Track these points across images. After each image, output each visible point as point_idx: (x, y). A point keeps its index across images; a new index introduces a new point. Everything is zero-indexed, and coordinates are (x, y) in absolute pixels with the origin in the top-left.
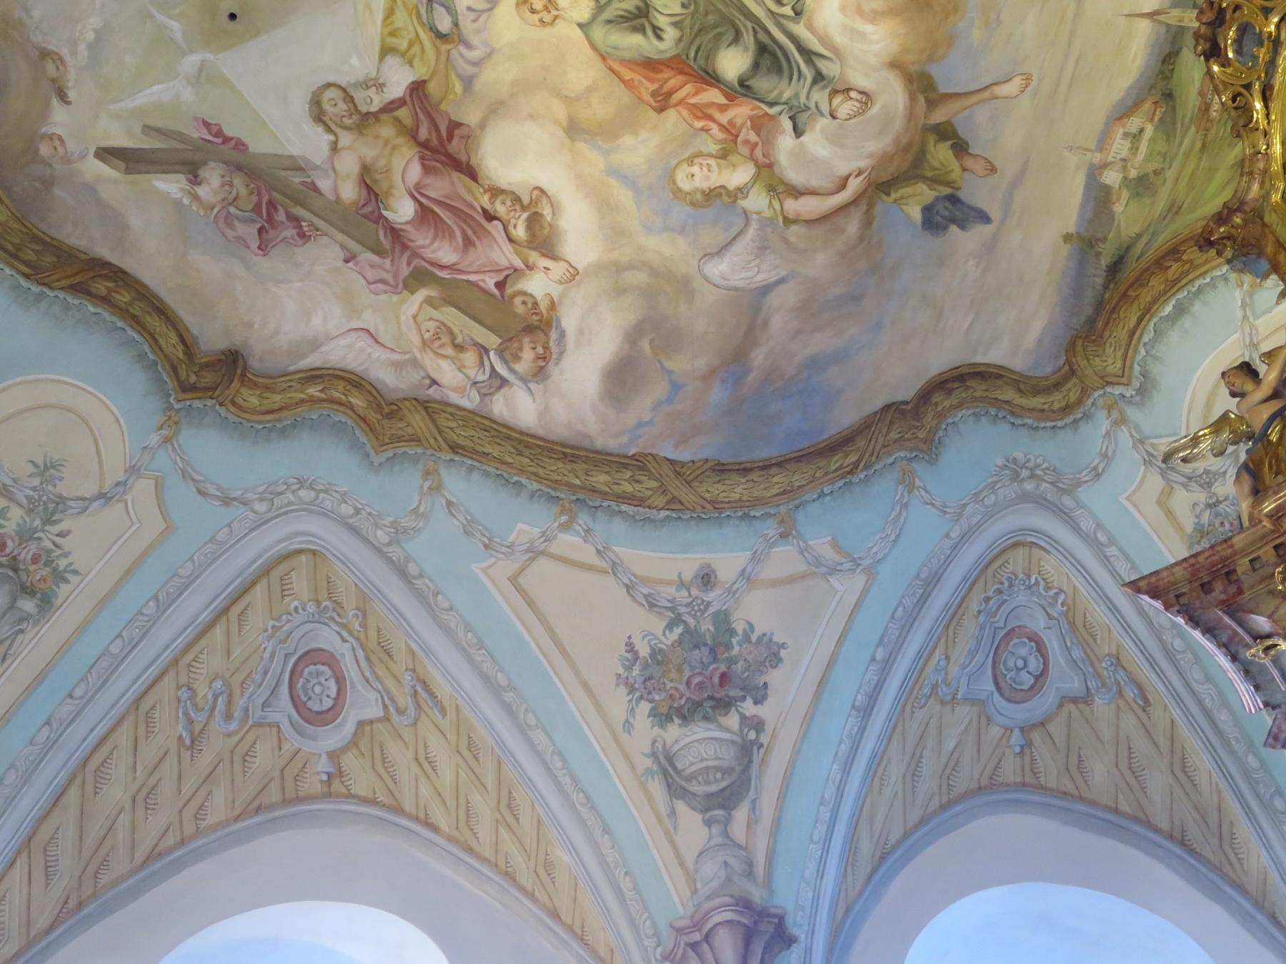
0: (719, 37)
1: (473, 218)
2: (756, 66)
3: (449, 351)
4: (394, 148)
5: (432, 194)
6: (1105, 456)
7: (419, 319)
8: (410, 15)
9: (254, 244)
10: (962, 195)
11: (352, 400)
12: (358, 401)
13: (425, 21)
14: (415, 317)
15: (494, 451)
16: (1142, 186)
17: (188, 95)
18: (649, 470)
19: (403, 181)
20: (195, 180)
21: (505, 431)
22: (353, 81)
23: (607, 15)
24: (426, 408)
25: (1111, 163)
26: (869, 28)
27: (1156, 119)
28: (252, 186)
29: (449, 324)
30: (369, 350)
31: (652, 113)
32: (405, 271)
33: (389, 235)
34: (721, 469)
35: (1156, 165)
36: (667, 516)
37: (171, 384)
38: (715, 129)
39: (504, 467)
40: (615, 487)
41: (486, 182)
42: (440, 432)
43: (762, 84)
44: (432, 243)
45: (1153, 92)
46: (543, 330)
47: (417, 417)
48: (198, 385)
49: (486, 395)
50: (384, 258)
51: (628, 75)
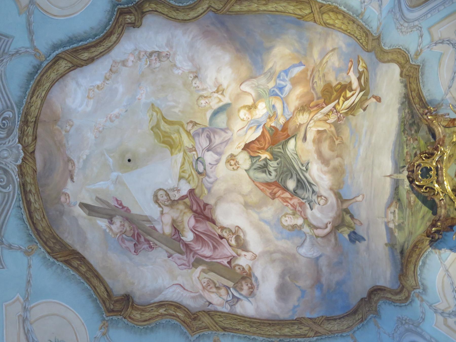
0: (287, 175)
1: (216, 239)
2: (297, 186)
3: (214, 290)
4: (184, 213)
5: (199, 230)
6: (422, 312)
7: (200, 278)
8: (190, 165)
9: (133, 251)
10: (356, 231)
11: (178, 314)
12: (180, 314)
13: (195, 168)
14: (198, 278)
15: (241, 327)
16: (400, 227)
17: (112, 188)
18: (303, 324)
19: (188, 226)
20: (111, 222)
21: (243, 318)
22: (169, 188)
23: (255, 167)
24: (209, 314)
25: (390, 221)
26: (324, 176)
27: (397, 207)
28: (131, 227)
29: (212, 279)
30: (182, 293)
31: (271, 199)
32: (192, 260)
33: (184, 246)
34: (328, 319)
35: (402, 221)
36: (317, 339)
37: (103, 309)
38: (290, 206)
39: (247, 333)
40: (293, 332)
41: (219, 225)
42: (217, 323)
43: (299, 192)
44: (201, 249)
45: (395, 199)
46: (248, 278)
47: (206, 318)
48: (114, 310)
49: (232, 305)
50: (183, 255)
51: (262, 187)
